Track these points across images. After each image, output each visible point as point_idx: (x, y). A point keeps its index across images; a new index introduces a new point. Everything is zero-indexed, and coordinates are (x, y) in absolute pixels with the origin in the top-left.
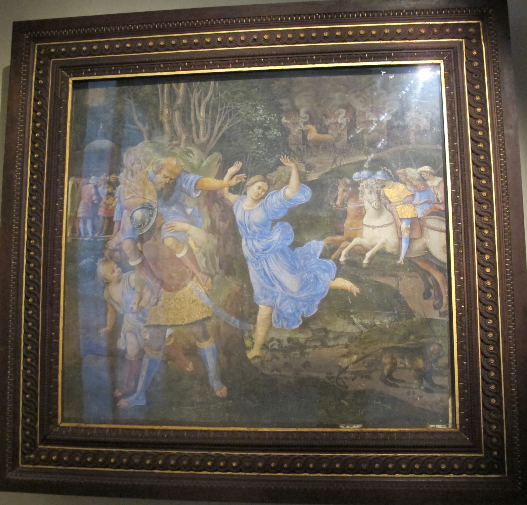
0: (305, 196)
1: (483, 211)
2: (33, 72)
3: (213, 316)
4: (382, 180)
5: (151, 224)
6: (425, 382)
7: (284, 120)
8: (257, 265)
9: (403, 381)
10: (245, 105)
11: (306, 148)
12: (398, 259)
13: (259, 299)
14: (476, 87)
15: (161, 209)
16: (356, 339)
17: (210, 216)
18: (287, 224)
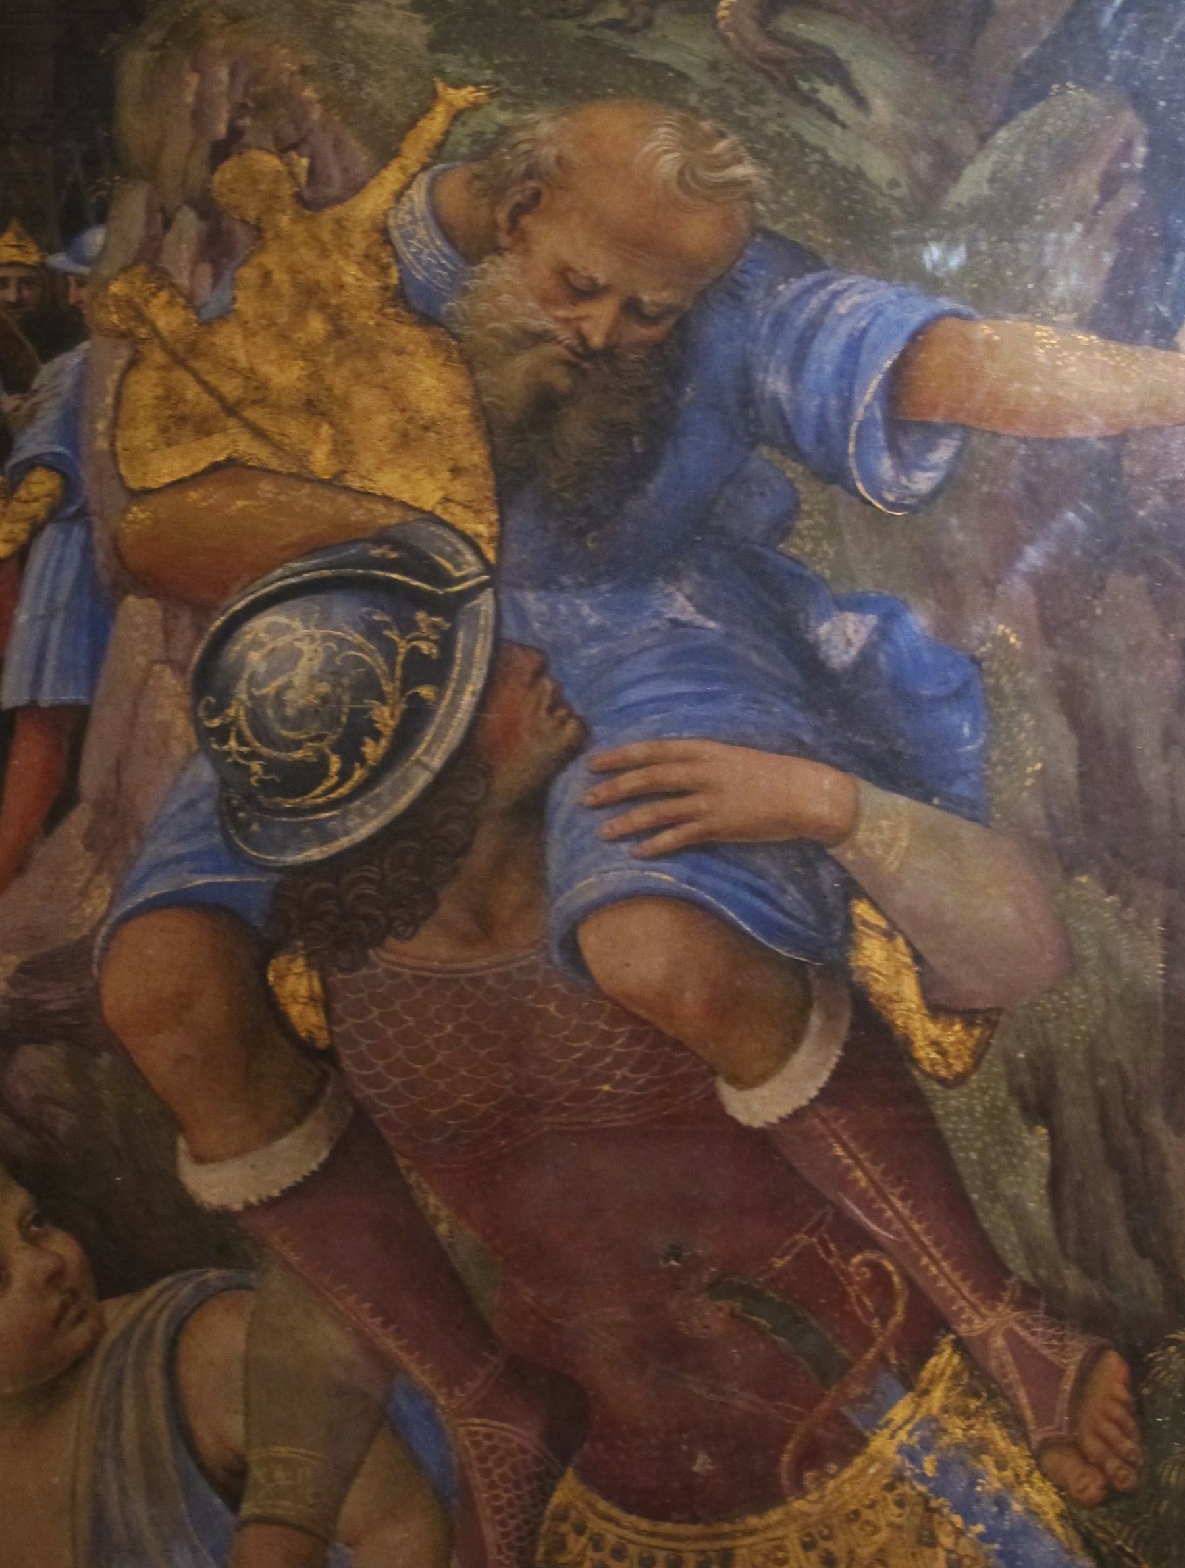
5: (433, 753)
15: (531, 600)
17: (1072, 696)
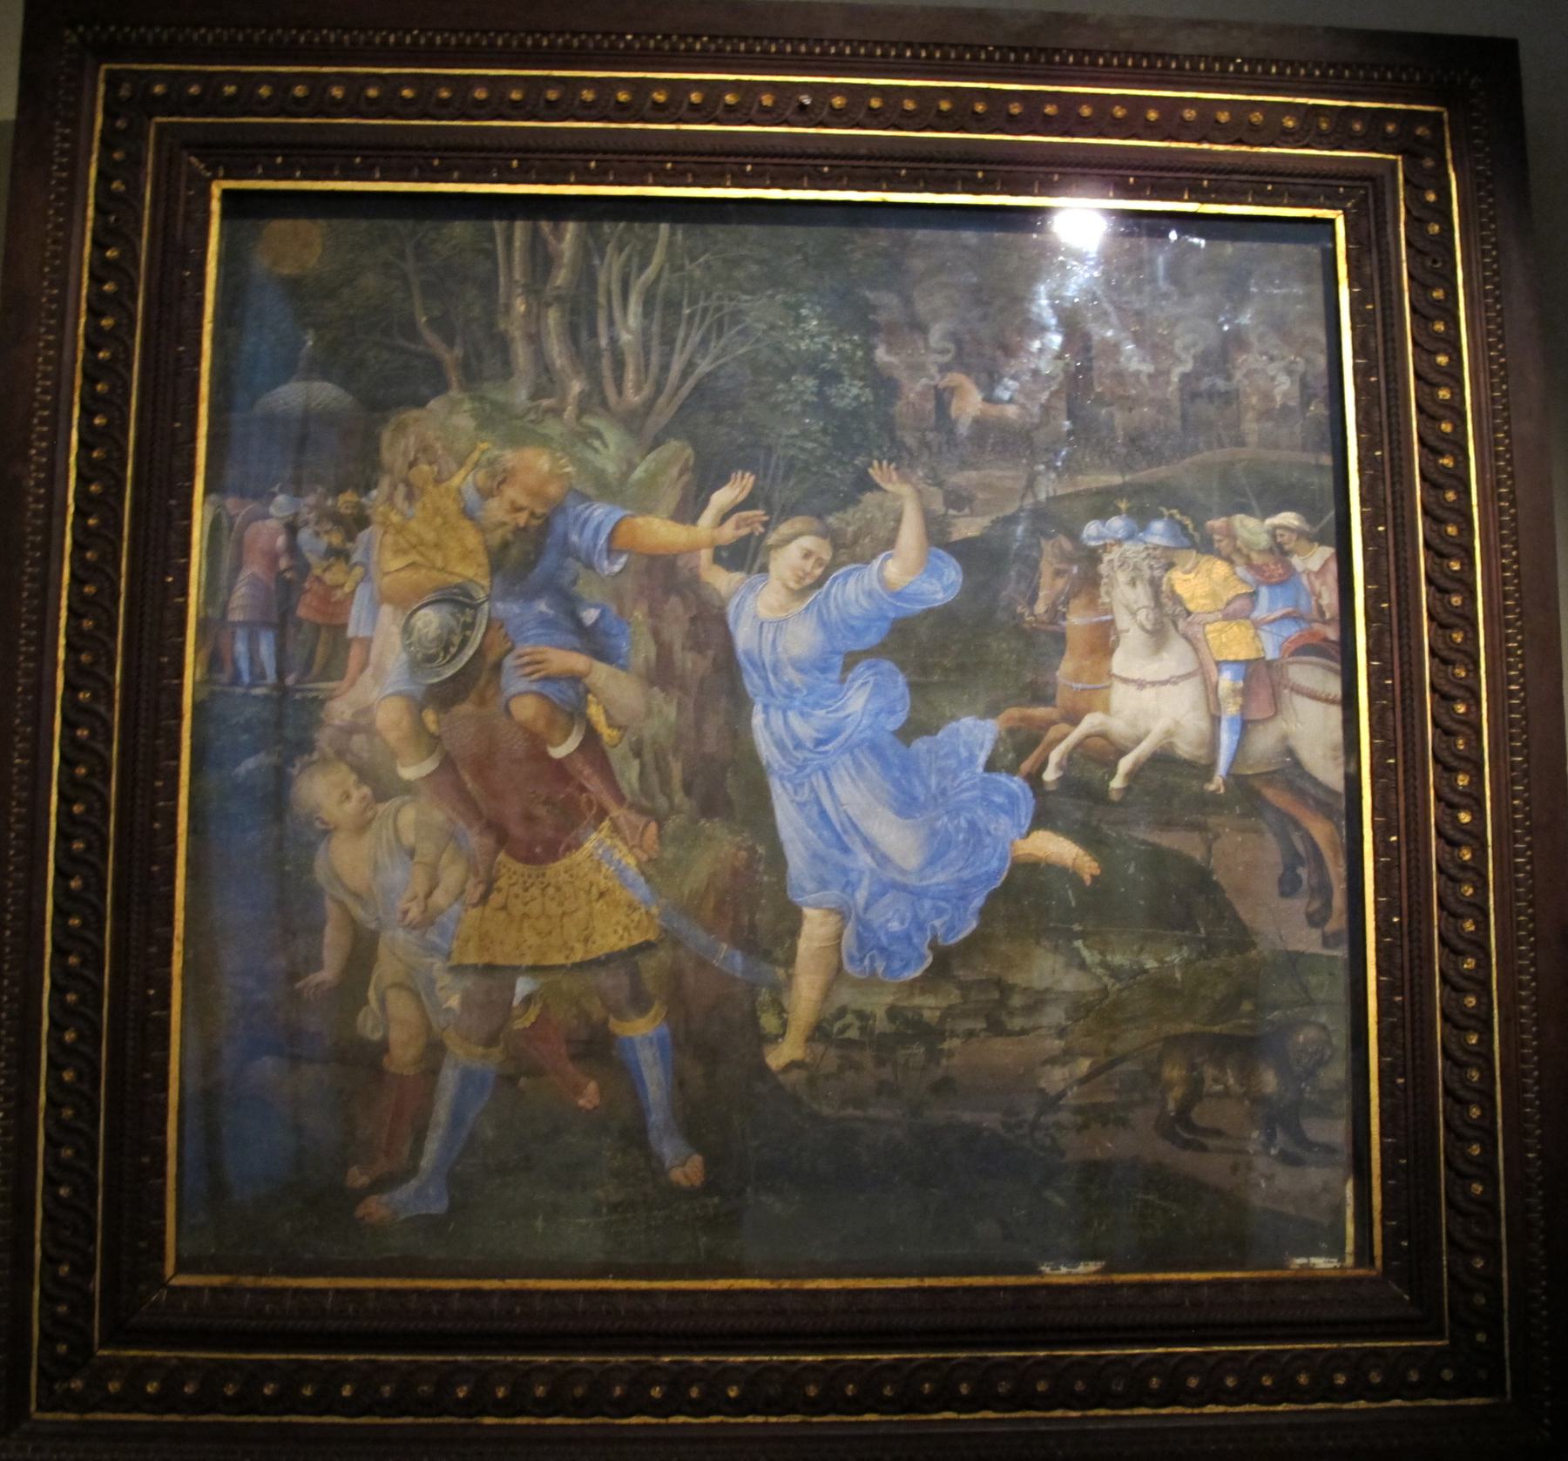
0: (942, 585)
1: (1450, 649)
2: (90, 153)
3: (662, 941)
4: (1166, 548)
5: (469, 652)
6: (1281, 1137)
7: (881, 354)
8: (797, 788)
9: (1218, 1133)
10: (764, 300)
11: (940, 441)
12: (1209, 779)
13: (803, 890)
14: (1435, 294)
15: (500, 605)
16: (1088, 1011)
17: (656, 634)
18: (887, 665)
